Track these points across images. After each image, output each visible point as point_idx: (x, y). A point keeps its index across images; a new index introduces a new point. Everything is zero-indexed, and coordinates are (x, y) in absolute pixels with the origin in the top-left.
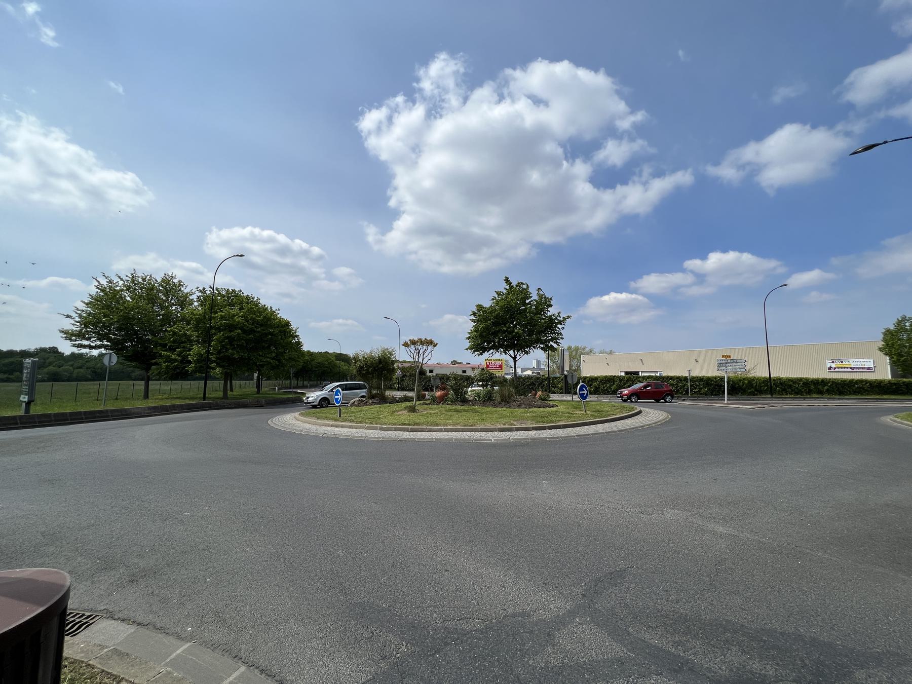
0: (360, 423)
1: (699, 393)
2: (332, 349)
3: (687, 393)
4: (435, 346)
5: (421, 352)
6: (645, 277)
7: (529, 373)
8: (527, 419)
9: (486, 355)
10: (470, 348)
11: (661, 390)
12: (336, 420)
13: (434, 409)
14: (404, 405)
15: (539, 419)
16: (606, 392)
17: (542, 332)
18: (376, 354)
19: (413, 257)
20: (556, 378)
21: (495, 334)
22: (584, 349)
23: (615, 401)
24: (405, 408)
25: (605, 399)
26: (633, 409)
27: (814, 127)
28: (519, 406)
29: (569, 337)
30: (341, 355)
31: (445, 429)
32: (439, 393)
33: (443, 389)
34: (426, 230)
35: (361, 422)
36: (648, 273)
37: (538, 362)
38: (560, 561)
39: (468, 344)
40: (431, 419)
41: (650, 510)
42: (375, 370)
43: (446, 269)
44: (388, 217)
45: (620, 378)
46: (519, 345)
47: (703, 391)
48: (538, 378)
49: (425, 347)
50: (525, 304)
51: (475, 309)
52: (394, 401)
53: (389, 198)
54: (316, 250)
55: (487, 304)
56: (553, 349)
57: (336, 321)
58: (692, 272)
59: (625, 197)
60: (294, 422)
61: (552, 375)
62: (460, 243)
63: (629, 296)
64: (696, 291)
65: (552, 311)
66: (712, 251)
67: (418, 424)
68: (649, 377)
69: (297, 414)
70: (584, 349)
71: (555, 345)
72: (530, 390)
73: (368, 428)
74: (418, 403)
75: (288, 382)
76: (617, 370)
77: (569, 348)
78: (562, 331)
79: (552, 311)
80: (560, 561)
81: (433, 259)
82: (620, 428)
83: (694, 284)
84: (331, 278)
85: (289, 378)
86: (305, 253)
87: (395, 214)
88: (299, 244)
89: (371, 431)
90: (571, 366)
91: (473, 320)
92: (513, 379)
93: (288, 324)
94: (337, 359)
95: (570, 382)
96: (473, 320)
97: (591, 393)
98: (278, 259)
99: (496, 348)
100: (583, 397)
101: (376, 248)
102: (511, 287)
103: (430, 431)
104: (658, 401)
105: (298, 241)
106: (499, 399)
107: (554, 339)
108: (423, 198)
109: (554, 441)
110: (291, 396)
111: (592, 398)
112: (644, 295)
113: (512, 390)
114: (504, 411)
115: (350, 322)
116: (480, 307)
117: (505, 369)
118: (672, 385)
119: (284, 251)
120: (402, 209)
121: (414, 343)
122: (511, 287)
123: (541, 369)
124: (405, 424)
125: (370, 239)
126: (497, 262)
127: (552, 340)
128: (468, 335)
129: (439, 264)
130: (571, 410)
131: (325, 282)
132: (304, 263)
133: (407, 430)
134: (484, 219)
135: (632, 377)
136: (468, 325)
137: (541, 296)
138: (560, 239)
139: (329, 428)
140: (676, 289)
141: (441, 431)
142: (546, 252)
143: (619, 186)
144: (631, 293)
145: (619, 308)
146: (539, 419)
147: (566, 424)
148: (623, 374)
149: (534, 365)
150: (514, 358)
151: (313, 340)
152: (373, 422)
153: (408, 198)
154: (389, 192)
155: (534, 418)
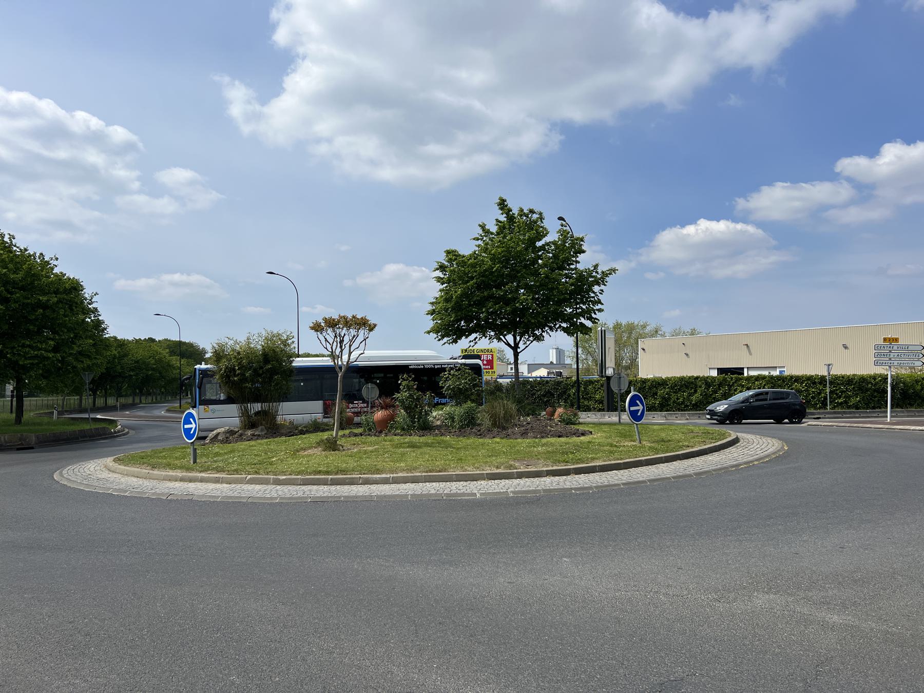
0: (235, 472)
1: (845, 405)
2: (164, 332)
3: (824, 405)
4: (371, 330)
5: (346, 339)
6: (765, 189)
7: (542, 372)
8: (538, 456)
9: (464, 343)
10: (435, 330)
11: (783, 402)
12: (188, 469)
13: (372, 443)
14: (314, 438)
15: (559, 457)
16: (682, 407)
17: (565, 300)
18: (258, 345)
19: (323, 149)
20: (591, 382)
21: (480, 304)
22: (644, 327)
23: (701, 422)
24: (319, 444)
25: (680, 420)
26: (723, 436)
27: (718, 221)
28: (524, 434)
29: (613, 308)
30: (180, 343)
31: (395, 476)
32: (379, 414)
33: (385, 407)
34: (346, 96)
35: (236, 471)
36: (770, 183)
37: (560, 353)
38: (585, 672)
39: (429, 323)
40: (366, 462)
41: (732, 595)
42: (256, 373)
43: (387, 174)
44: (270, 66)
45: (708, 381)
46: (527, 324)
47: (853, 401)
48: (559, 383)
49: (353, 332)
50: (536, 250)
51: (443, 258)
52: (295, 430)
53: (273, 27)
54: (119, 133)
55: (467, 248)
56: (585, 330)
57: (167, 277)
58: (849, 180)
59: (726, 35)
60: (105, 475)
61: (584, 378)
62: (414, 121)
63: (731, 225)
64: (855, 215)
65: (584, 262)
66: (889, 141)
67: (343, 471)
68: (758, 378)
69: (109, 461)
70: (644, 327)
71: (588, 323)
72: (547, 404)
73: (251, 482)
74: (341, 433)
75: (74, 400)
76: (703, 366)
77: (617, 326)
78: (601, 297)
79: (584, 262)
80: (585, 672)
81: (361, 152)
82: (697, 470)
83: (851, 203)
84: (155, 190)
85: (77, 391)
86: (95, 139)
87: (283, 62)
88: (83, 120)
89: (258, 487)
90: (618, 364)
91: (439, 279)
92: (512, 385)
93: (75, 287)
94: (172, 353)
95: (615, 389)
96: (439, 279)
97: (651, 409)
98: (35, 146)
99: (481, 329)
100: (635, 416)
101: (246, 129)
102: (511, 218)
103: (367, 482)
104: (779, 421)
105: (81, 115)
106: (487, 423)
107: (588, 314)
108: (346, 31)
109: (584, 493)
110: (86, 427)
111: (656, 419)
112: (759, 225)
113: (513, 407)
114: (498, 443)
115: (195, 278)
116: (452, 255)
117: (499, 368)
118: (799, 391)
119: (54, 133)
120: (301, 50)
121: (331, 324)
122: (511, 218)
123: (564, 366)
124: (319, 472)
125: (236, 111)
126: (484, 161)
127: (582, 314)
128: (430, 308)
129: (373, 163)
130: (615, 440)
131: (141, 199)
132: (93, 157)
133: (324, 483)
134: (463, 75)
135: (731, 377)
136: (432, 289)
137: (564, 234)
138: (605, 115)
139: (178, 484)
140: (819, 212)
141: (385, 481)
142: (577, 141)
143: (714, 14)
144: (735, 220)
145: (714, 245)
146: (559, 457)
147: (607, 460)
148: (714, 373)
149: (553, 357)
150: (515, 348)
151: (125, 318)
152: (260, 470)
153: (314, 28)
154: (275, 14)
155: (549, 456)
